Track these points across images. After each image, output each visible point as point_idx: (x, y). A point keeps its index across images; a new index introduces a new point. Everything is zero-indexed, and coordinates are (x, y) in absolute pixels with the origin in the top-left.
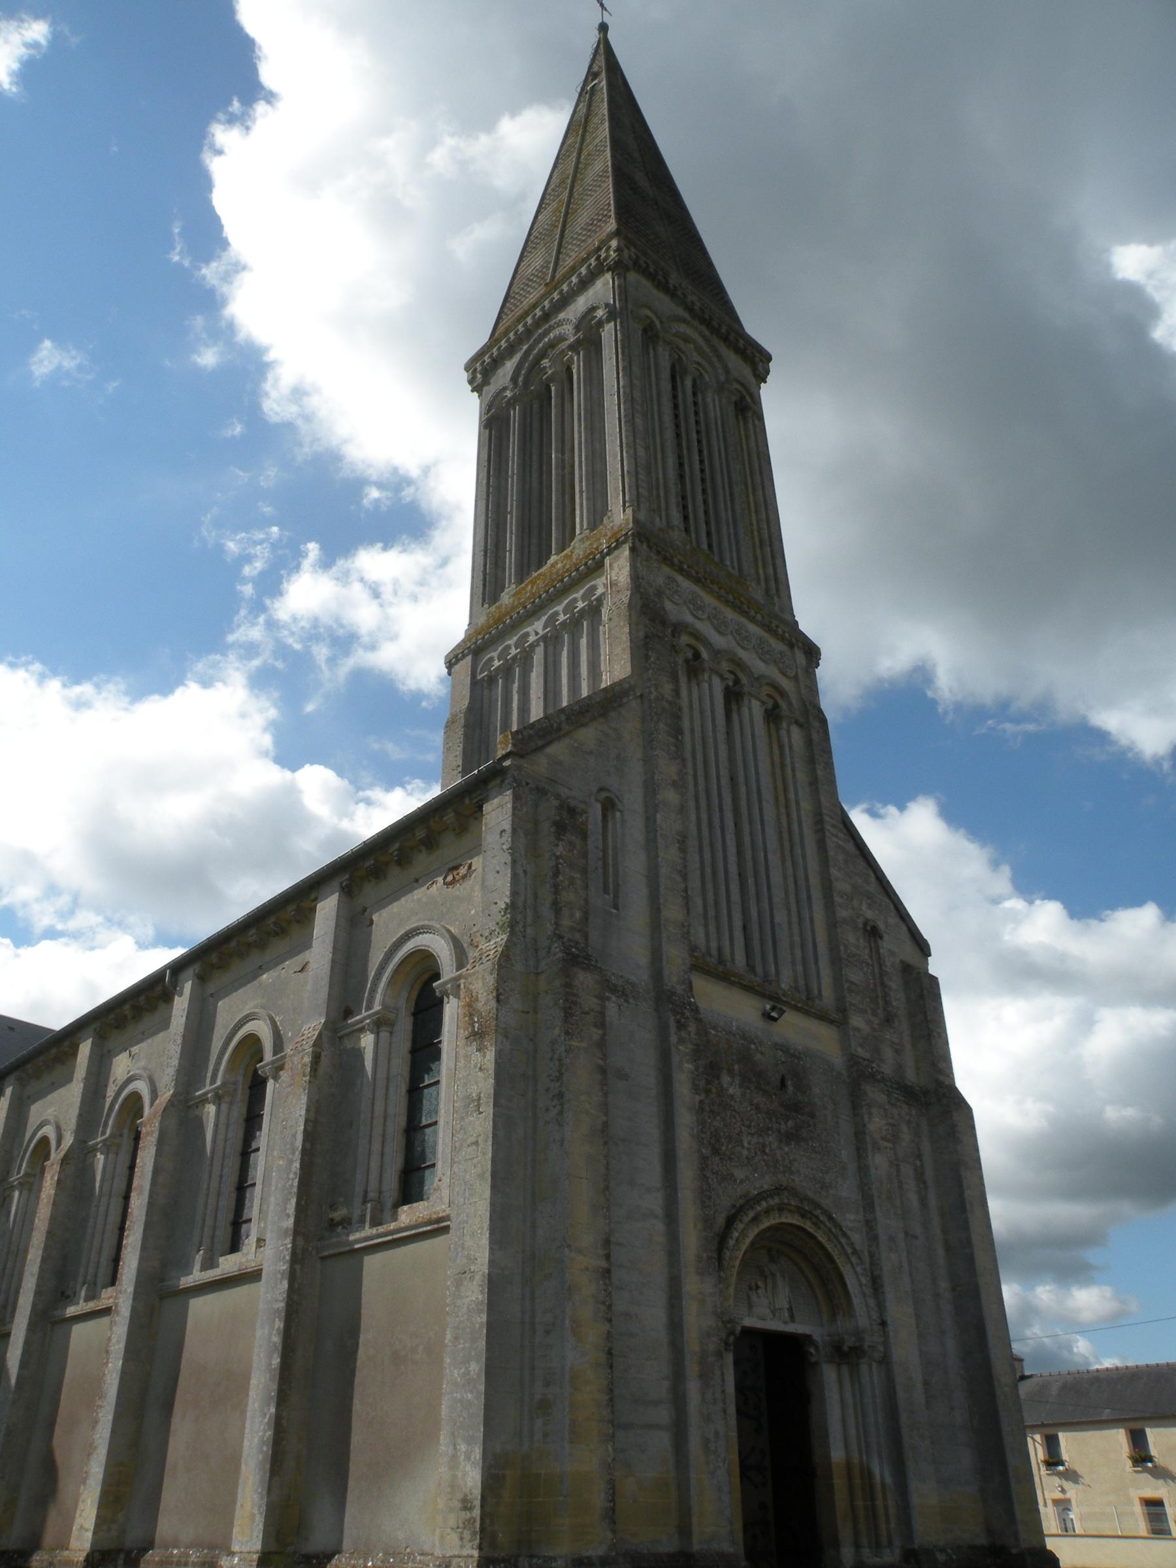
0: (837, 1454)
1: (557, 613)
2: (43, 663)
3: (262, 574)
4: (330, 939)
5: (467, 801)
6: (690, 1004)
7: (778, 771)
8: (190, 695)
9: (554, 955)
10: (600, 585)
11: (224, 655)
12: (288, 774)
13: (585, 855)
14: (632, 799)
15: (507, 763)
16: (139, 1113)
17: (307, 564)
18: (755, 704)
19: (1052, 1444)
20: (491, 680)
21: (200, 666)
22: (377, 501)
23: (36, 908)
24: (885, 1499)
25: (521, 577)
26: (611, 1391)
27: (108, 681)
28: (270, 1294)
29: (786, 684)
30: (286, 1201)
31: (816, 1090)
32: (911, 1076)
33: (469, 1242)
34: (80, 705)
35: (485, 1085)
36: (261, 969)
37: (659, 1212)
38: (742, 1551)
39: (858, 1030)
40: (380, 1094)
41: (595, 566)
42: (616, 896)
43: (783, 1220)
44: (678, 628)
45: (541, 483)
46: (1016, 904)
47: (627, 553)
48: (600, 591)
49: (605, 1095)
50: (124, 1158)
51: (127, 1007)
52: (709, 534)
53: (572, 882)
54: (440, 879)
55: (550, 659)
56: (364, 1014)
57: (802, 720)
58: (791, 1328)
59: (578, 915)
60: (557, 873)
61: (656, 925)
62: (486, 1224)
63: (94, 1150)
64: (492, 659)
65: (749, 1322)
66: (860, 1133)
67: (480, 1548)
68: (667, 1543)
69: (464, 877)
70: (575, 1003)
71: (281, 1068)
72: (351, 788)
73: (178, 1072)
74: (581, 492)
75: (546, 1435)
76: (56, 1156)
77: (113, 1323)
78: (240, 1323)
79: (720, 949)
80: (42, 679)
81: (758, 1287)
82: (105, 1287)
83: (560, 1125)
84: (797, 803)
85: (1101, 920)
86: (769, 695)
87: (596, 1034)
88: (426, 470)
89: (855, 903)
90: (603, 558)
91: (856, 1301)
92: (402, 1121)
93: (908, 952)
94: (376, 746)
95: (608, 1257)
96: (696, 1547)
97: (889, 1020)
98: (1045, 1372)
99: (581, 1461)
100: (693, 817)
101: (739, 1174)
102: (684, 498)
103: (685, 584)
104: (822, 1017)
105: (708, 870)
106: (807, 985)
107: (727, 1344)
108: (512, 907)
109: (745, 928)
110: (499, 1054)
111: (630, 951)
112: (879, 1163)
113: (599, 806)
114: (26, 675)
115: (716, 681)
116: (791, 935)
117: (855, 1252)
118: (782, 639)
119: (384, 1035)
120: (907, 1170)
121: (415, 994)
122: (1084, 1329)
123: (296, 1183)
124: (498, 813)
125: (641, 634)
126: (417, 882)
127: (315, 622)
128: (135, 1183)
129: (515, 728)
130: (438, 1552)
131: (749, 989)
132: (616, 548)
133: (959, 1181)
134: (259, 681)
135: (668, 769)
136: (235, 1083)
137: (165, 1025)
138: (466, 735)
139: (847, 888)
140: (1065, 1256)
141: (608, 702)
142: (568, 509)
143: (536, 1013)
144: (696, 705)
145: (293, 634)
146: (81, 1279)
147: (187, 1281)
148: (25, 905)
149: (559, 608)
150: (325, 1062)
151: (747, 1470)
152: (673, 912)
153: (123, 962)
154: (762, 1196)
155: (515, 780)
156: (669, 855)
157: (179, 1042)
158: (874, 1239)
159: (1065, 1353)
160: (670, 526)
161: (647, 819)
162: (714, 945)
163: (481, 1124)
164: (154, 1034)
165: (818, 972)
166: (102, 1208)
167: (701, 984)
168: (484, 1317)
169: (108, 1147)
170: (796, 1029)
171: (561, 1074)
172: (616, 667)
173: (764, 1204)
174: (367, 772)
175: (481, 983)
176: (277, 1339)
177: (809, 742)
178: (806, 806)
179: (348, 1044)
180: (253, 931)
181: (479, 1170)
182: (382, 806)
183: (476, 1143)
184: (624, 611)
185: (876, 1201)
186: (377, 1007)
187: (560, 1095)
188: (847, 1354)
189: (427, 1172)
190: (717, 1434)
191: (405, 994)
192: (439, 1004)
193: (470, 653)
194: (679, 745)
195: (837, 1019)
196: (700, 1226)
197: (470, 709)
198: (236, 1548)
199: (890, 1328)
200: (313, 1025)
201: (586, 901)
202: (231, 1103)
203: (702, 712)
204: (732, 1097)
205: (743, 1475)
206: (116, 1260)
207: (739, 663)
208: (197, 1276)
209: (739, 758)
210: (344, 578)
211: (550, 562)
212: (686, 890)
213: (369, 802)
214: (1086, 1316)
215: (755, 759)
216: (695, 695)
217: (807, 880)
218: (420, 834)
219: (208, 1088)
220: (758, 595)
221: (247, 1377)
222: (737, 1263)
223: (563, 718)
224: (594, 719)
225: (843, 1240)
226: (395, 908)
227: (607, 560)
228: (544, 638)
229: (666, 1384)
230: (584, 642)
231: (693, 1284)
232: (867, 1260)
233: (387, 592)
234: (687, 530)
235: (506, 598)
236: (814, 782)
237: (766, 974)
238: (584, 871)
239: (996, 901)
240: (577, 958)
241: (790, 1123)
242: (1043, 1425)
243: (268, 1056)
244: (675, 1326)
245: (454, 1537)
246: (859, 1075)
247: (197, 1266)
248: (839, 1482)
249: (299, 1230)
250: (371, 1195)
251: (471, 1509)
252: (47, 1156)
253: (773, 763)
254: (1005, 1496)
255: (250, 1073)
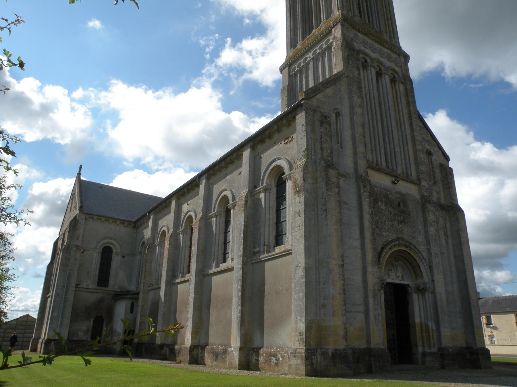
0: (417, 320)
1: (316, 50)
2: (146, 85)
3: (213, 50)
4: (248, 164)
5: (290, 116)
6: (367, 179)
7: (395, 99)
8: (193, 91)
9: (322, 165)
10: (331, 38)
11: (202, 77)
12: (227, 115)
13: (330, 131)
14: (345, 111)
15: (303, 102)
16: (192, 222)
17: (227, 45)
18: (387, 77)
19: (489, 319)
20: (295, 75)
21: (195, 82)
22: (248, 23)
23: (152, 164)
24: (433, 333)
25: (303, 38)
26: (345, 301)
27: (166, 89)
28: (237, 275)
29: (397, 69)
30: (240, 246)
31: (410, 207)
32: (443, 201)
33: (298, 257)
34: (159, 98)
35: (301, 208)
36: (226, 175)
37: (359, 247)
38: (386, 348)
39: (425, 186)
40: (267, 213)
41: (329, 32)
42: (341, 145)
43: (400, 248)
44: (359, 52)
45: (308, 4)
46: (477, 145)
47: (340, 26)
48: (331, 41)
49: (340, 210)
50: (188, 236)
51: (185, 189)
52: (368, 17)
53: (327, 140)
54: (283, 142)
55: (315, 66)
56: (261, 187)
57: (403, 81)
58: (402, 282)
59: (329, 151)
60: (321, 138)
61: (355, 154)
62: (303, 251)
63: (179, 234)
64: (295, 67)
65: (389, 280)
66: (425, 220)
67: (306, 346)
68: (363, 345)
69: (291, 141)
70: (329, 180)
71: (235, 206)
72: (248, 118)
73: (203, 208)
74: (323, 6)
75: (324, 314)
76: (168, 236)
77: (190, 284)
78: (228, 283)
79: (377, 161)
80: (146, 91)
81: (391, 270)
82: (186, 274)
83: (326, 219)
84: (402, 110)
85: (507, 150)
86: (392, 74)
87: (337, 190)
88: (262, 11)
89: (423, 144)
90: (332, 29)
91: (424, 274)
92: (275, 220)
93: (442, 160)
94: (254, 104)
95: (343, 261)
96: (372, 346)
97: (435, 183)
98: (487, 297)
99: (336, 322)
100: (366, 117)
101: (385, 234)
102: (359, 5)
103: (361, 36)
104: (412, 182)
105: (372, 135)
106: (407, 172)
107: (381, 287)
108: (307, 150)
109: (385, 154)
110: (305, 198)
111: (347, 162)
112: (432, 230)
113: (334, 115)
114: (141, 90)
115: (373, 69)
116: (401, 156)
117: (424, 258)
118: (396, 53)
119: (267, 193)
120: (442, 232)
121: (277, 180)
122: (499, 284)
123: (242, 241)
124: (301, 119)
125: (346, 55)
126: (275, 143)
127: (231, 65)
128: (193, 243)
129: (304, 90)
130: (293, 347)
131: (387, 174)
132: (336, 25)
133: (459, 236)
134: (215, 85)
135: (357, 101)
136: (221, 211)
137: (198, 194)
138: (288, 94)
139: (420, 139)
140: (494, 262)
141: (335, 80)
142: (318, 12)
143: (316, 184)
144: (366, 79)
145: (224, 70)
146: (179, 272)
147: (211, 271)
148: (149, 163)
149: (317, 48)
150: (249, 203)
151: (388, 325)
152: (361, 149)
153: (181, 177)
154: (393, 241)
155: (306, 108)
156: (359, 130)
157: (202, 199)
158: (430, 254)
159: (493, 292)
160: (354, 15)
161: (351, 118)
162: (375, 160)
163: (300, 220)
164: (194, 197)
165: (410, 167)
166: (183, 251)
167: (371, 172)
168: (304, 280)
169: (183, 232)
170: (403, 186)
171: (326, 203)
172: (338, 66)
173: (393, 243)
174: (254, 112)
175: (298, 175)
176: (240, 288)
177: (406, 89)
178: (405, 111)
179: (256, 197)
180: (223, 163)
181: (300, 234)
182: (259, 123)
183: (299, 226)
184: (340, 47)
185: (431, 242)
186: (265, 185)
187: (326, 210)
188: (421, 290)
189: (284, 236)
190: (379, 314)
191: (273, 180)
192: (285, 183)
193: (287, 66)
194: (361, 92)
195: (417, 183)
196: (372, 251)
197: (289, 85)
198: (232, 346)
199: (435, 282)
200: (244, 192)
201: (332, 146)
202: (220, 218)
203: (368, 80)
204: (382, 209)
205: (387, 326)
206: (189, 266)
207: (381, 63)
208: (214, 270)
209: (382, 96)
210: (240, 50)
211: (313, 32)
212: (365, 141)
213: (254, 122)
214: (501, 280)
215: (387, 96)
216: (366, 75)
217: (406, 136)
218: (275, 127)
219: (212, 213)
220: (386, 37)
221: (232, 299)
222: (385, 262)
223: (321, 85)
224: (331, 85)
225: (420, 255)
226: (268, 152)
227: (333, 30)
228: (313, 59)
229: (362, 299)
230: (326, 59)
231: (370, 269)
232: (428, 260)
233: (254, 53)
234: (361, 16)
235: (299, 46)
236: (408, 103)
237: (393, 169)
238: (330, 137)
239: (468, 144)
240: (329, 166)
241: (402, 217)
242: (486, 313)
243: (231, 202)
244: (365, 282)
245: (297, 343)
246: (425, 201)
247: (214, 267)
248: (418, 329)
249: (244, 255)
250: (266, 244)
251: (302, 335)
252: (165, 236)
253: (393, 97)
254: (473, 333)
255: (225, 208)
